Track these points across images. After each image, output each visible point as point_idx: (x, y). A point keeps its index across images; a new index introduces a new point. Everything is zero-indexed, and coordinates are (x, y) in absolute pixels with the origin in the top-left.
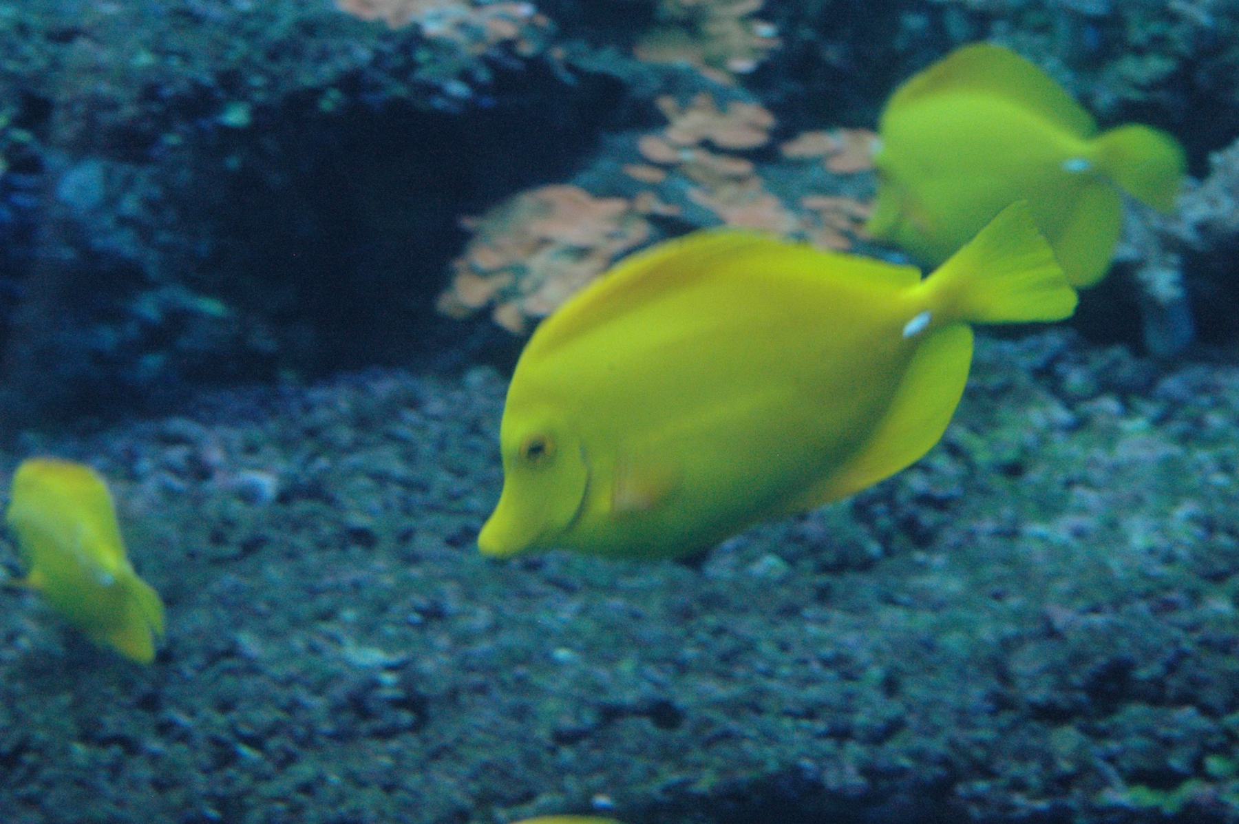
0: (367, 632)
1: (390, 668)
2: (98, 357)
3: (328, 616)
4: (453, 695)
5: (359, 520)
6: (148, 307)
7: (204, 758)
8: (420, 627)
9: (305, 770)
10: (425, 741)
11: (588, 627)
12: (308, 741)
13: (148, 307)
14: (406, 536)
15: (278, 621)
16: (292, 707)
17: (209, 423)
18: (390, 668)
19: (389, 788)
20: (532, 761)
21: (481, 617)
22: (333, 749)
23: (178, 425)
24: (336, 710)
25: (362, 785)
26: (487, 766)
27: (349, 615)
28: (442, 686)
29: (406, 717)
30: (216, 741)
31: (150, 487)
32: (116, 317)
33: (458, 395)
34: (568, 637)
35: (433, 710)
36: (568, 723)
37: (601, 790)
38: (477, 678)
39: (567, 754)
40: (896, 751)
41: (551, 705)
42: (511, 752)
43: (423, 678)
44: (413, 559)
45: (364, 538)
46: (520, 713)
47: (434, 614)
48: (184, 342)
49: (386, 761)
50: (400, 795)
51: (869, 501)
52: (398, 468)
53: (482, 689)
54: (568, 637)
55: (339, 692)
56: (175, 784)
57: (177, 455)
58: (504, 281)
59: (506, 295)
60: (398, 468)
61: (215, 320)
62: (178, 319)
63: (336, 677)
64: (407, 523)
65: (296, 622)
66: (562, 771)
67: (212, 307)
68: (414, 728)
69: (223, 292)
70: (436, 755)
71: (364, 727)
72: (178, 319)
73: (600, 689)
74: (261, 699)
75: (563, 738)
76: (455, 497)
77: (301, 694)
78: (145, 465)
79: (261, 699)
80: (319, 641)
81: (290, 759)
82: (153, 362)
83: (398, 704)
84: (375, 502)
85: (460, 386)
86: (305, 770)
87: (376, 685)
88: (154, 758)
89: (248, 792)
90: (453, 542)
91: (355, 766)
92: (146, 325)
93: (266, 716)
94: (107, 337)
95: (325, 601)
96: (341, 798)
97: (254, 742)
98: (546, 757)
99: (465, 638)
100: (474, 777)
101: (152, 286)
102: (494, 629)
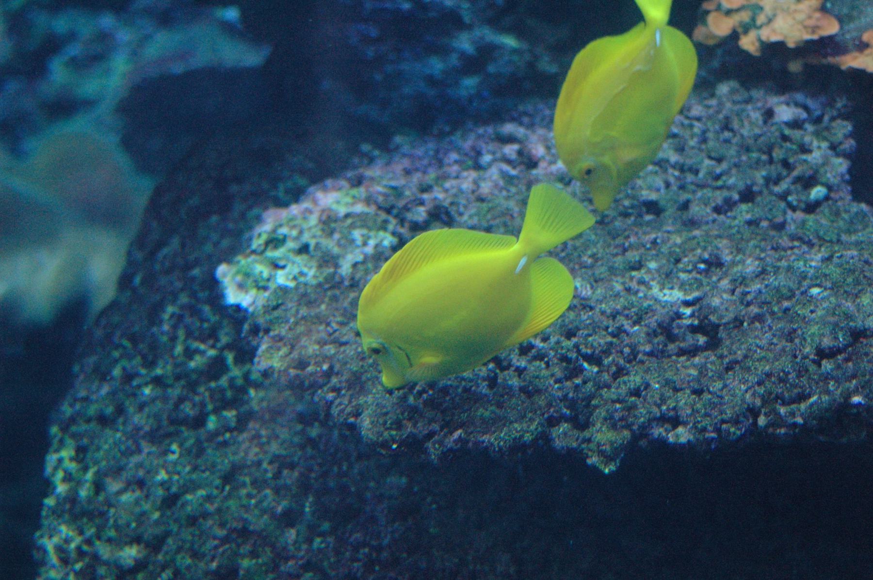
0: (667, 277)
1: (687, 304)
2: (431, 80)
3: (638, 266)
4: (738, 322)
5: (647, 195)
6: (465, 43)
7: (558, 371)
8: (706, 272)
9: (635, 379)
10: (721, 357)
11: (833, 270)
12: (633, 357)
13: (465, 43)
14: (685, 206)
15: (601, 270)
16: (619, 332)
17: (531, 126)
18: (687, 304)
19: (698, 392)
20: (802, 372)
21: (751, 266)
22: (652, 363)
23: (509, 128)
24: (652, 335)
25: (676, 390)
26: (769, 375)
27: (653, 265)
28: (729, 317)
29: (702, 340)
30: (564, 359)
31: (494, 173)
32: (443, 51)
33: (713, 102)
34: (819, 279)
35: (722, 334)
36: (827, 342)
37: (856, 391)
38: (754, 310)
39: (827, 365)
40: (812, 323)
41: (814, 329)
42: (785, 364)
43: (715, 310)
44: (692, 223)
45: (653, 207)
46: (790, 336)
47: (715, 263)
48: (491, 69)
49: (694, 372)
50: (706, 396)
51: (460, 149)
52: (674, 158)
53: (759, 318)
54: (819, 279)
55: (652, 321)
56: (538, 391)
57: (510, 150)
58: (745, 16)
59: (746, 28)
60: (674, 158)
61: (515, 51)
62: (487, 52)
63: (649, 310)
64: (685, 196)
65: (612, 270)
66: (826, 378)
67: (510, 41)
68: (708, 347)
69: (518, 30)
70: (729, 368)
71: (672, 347)
72: (487, 52)
73: (848, 317)
74: (595, 328)
75: (822, 354)
76: (718, 177)
77: (622, 321)
78: (487, 158)
79: (595, 328)
80: (634, 285)
81: (620, 372)
82: (470, 83)
83: (694, 329)
84: (659, 182)
85: (713, 95)
86: (635, 379)
87: (679, 316)
88: (520, 371)
89: (592, 397)
90: (717, 210)
91: (669, 375)
92: (463, 55)
93: (600, 340)
94: (436, 65)
95: (633, 256)
96: (663, 400)
97: (592, 359)
98: (812, 368)
99: (743, 280)
100: (760, 383)
101: (469, 27)
102: (762, 273)
